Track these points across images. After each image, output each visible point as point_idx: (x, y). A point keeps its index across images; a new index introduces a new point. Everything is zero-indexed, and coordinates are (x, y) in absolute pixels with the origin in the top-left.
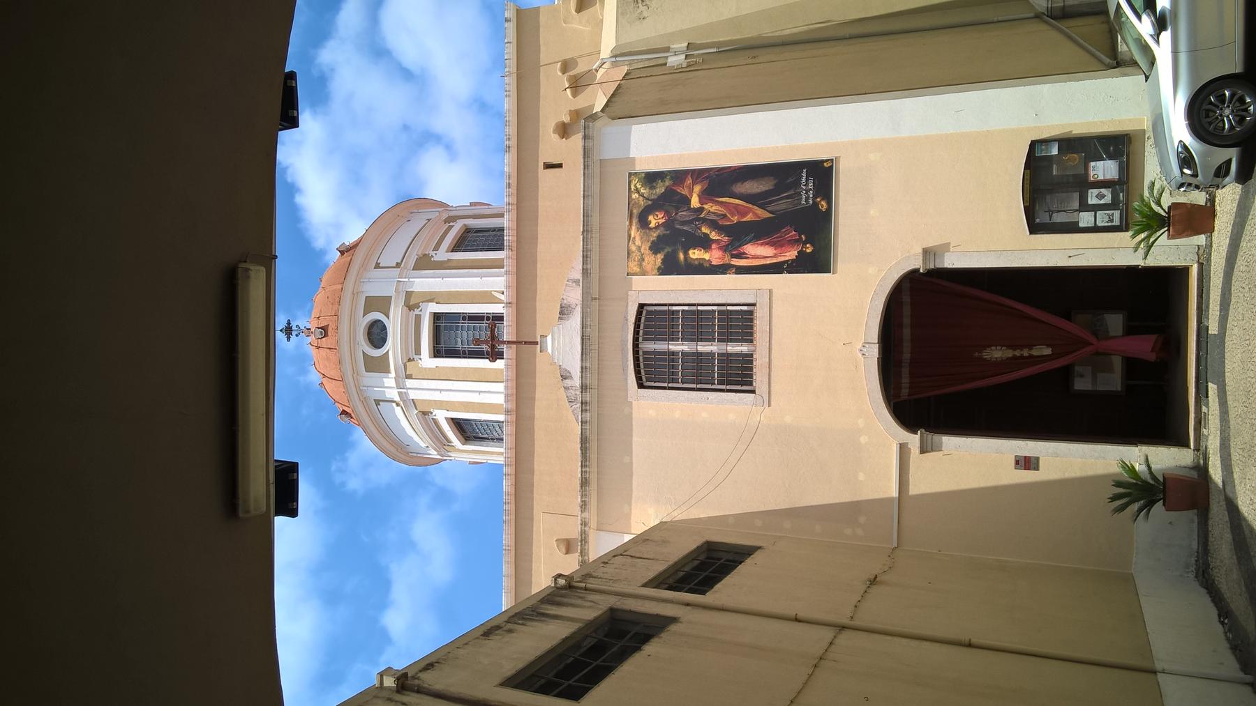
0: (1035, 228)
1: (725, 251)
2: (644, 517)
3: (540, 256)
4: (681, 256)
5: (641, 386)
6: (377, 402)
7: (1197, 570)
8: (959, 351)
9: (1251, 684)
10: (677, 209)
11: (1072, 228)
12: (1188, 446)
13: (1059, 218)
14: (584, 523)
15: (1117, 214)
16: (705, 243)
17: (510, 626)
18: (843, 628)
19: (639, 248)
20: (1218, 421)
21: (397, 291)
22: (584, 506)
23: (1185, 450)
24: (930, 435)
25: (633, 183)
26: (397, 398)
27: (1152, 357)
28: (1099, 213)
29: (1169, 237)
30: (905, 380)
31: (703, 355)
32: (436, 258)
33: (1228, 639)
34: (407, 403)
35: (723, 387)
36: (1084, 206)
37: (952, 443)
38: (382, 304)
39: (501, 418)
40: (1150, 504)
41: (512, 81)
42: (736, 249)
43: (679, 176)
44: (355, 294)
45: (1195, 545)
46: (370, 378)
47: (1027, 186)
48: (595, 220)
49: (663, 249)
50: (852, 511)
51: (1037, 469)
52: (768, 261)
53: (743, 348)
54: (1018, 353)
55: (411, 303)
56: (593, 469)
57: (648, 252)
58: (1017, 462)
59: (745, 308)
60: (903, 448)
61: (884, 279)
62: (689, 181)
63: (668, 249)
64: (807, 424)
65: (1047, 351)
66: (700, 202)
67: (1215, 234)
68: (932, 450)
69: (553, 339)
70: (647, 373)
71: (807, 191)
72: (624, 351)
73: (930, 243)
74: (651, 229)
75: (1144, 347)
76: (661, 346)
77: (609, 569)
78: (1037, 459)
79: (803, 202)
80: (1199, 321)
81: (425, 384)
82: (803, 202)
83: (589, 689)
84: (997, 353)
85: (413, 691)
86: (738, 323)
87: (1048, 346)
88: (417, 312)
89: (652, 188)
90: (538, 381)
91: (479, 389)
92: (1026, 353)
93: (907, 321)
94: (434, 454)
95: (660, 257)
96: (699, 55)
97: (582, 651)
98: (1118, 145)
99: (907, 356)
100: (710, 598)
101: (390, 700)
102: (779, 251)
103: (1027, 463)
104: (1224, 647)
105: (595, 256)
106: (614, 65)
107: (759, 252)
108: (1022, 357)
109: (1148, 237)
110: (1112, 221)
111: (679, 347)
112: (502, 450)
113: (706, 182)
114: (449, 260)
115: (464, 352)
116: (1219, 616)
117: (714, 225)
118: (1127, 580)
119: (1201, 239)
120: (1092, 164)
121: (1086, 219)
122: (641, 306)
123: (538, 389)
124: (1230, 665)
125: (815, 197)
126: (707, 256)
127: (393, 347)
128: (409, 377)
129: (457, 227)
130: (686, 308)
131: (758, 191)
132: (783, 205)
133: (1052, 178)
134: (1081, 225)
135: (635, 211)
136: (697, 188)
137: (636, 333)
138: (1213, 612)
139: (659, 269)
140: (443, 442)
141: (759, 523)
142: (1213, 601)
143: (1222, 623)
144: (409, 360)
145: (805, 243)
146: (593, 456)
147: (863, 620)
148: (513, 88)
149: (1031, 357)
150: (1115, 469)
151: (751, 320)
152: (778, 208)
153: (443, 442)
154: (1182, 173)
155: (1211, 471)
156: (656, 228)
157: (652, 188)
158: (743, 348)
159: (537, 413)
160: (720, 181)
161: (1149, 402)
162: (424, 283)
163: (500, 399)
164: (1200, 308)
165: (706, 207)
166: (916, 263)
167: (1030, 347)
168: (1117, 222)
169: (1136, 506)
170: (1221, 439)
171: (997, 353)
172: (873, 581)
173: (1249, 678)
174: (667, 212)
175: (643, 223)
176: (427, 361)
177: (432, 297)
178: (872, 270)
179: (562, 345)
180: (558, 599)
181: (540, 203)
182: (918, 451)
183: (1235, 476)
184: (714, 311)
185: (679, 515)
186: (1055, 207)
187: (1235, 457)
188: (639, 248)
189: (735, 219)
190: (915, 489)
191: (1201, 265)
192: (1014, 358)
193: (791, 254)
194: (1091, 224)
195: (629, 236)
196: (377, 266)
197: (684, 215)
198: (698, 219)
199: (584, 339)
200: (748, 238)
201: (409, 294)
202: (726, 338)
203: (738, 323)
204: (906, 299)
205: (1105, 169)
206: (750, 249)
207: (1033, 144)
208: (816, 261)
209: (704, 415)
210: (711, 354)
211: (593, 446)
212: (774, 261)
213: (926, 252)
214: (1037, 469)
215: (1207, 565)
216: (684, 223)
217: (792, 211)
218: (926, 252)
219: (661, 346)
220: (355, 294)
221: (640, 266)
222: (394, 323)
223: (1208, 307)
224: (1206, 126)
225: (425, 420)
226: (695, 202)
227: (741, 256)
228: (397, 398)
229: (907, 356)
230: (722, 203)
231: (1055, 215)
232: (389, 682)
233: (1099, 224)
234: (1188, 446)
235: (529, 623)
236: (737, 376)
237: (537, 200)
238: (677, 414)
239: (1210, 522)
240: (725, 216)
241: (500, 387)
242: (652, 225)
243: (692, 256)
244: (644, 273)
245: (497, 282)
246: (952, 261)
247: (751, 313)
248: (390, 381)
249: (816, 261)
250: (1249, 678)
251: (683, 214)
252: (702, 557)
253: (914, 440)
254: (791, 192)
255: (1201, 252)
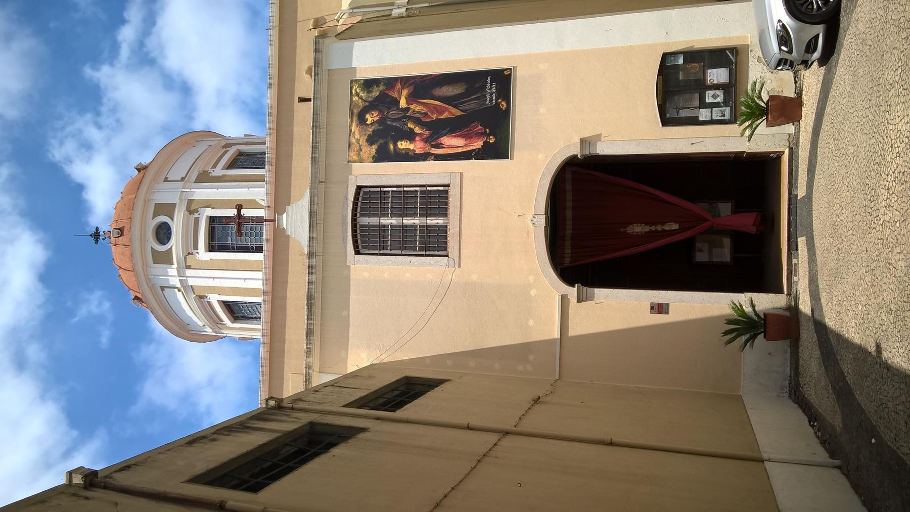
0: (666, 121)
1: (426, 142)
2: (358, 359)
3: (293, 171)
4: (392, 147)
5: (358, 252)
6: (163, 288)
7: (790, 391)
8: (607, 220)
9: (839, 468)
10: (389, 109)
11: (694, 121)
12: (782, 292)
13: (684, 113)
14: (309, 367)
15: (727, 111)
16: (410, 136)
17: (215, 436)
18: (507, 433)
19: (358, 141)
20: (807, 265)
21: (181, 199)
22: (309, 352)
23: (779, 296)
24: (585, 288)
25: (355, 88)
26: (179, 285)
27: (753, 230)
28: (714, 109)
29: (768, 126)
30: (568, 251)
31: (409, 225)
32: (214, 174)
33: (818, 437)
34: (187, 289)
35: (423, 253)
36: (703, 105)
37: (601, 293)
38: (168, 209)
39: (259, 300)
40: (753, 338)
41: (274, 34)
42: (434, 141)
43: (391, 82)
44: (146, 202)
45: (788, 370)
46: (157, 269)
47: (660, 89)
48: (323, 119)
49: (377, 141)
50: (523, 350)
51: (667, 313)
52: (460, 150)
53: (440, 221)
54: (653, 228)
55: (192, 208)
56: (317, 322)
57: (365, 143)
58: (652, 308)
59: (441, 188)
60: (564, 298)
61: (550, 163)
62: (399, 86)
63: (381, 141)
64: (488, 282)
65: (675, 227)
66: (407, 103)
67: (802, 123)
68: (587, 300)
69: (287, 216)
70: (363, 242)
71: (491, 94)
72: (344, 224)
73: (586, 134)
74: (368, 125)
75: (747, 222)
76: (374, 221)
77: (318, 396)
78: (668, 305)
79: (488, 102)
80: (790, 193)
81: (201, 273)
82: (488, 102)
83: (267, 485)
84: (638, 229)
85: (100, 488)
86: (435, 200)
87: (676, 222)
88: (196, 215)
89: (369, 92)
90: (290, 269)
91: (241, 276)
92: (659, 228)
93: (569, 204)
94: (209, 331)
95: (374, 147)
96: (416, 9)
97: (280, 457)
98: (727, 57)
99: (569, 232)
100: (400, 414)
101: (75, 495)
102: (468, 142)
103: (660, 308)
104: (815, 443)
105: (322, 146)
106: (351, 15)
107: (453, 143)
108: (656, 231)
109: (752, 124)
110: (724, 115)
111: (387, 221)
112: (259, 327)
113: (412, 87)
114: (224, 176)
115: (233, 247)
116: (810, 422)
117: (418, 122)
118: (739, 399)
119: (790, 128)
120: (709, 71)
121: (704, 114)
122: (359, 188)
123: (290, 275)
124: (822, 455)
125: (497, 98)
126: (411, 147)
127: (176, 244)
128: (189, 267)
129: (232, 151)
130: (395, 189)
131: (453, 94)
132: (472, 105)
133: (680, 82)
134: (701, 119)
135: (355, 111)
136: (405, 92)
137: (355, 209)
138: (805, 419)
139: (373, 157)
140: (216, 321)
141: (449, 362)
142: (803, 412)
143: (813, 426)
144: (189, 254)
145: (489, 135)
146: (317, 310)
147: (525, 427)
148: (276, 39)
149: (663, 231)
150: (727, 311)
151: (447, 198)
152: (468, 107)
153: (216, 321)
154: (780, 49)
155: (801, 307)
156: (372, 124)
157: (369, 92)
158: (440, 221)
159: (289, 294)
160: (423, 86)
161: (755, 265)
162: (203, 193)
163: (259, 285)
164: (790, 183)
165: (412, 107)
166: (575, 150)
167: (663, 224)
168: (727, 117)
169: (744, 338)
170: (810, 276)
171: (638, 229)
172: (537, 401)
173: (837, 462)
174: (381, 112)
175: (362, 120)
176: (203, 254)
177: (209, 204)
178: (541, 156)
179: (296, 221)
180: (266, 416)
181: (295, 129)
182: (575, 300)
183: (822, 301)
184: (416, 191)
185: (386, 358)
186: (681, 105)
187: (822, 284)
188: (358, 141)
189: (434, 117)
190: (573, 332)
191: (791, 149)
192: (651, 232)
193: (478, 144)
194: (708, 118)
195: (350, 131)
196: (166, 180)
197: (397, 114)
198: (405, 117)
199: (311, 214)
200: (444, 132)
201: (190, 202)
202: (427, 212)
203: (435, 200)
204: (569, 176)
205: (717, 75)
206: (447, 141)
207: (665, 56)
208: (498, 149)
209: (407, 275)
210: (414, 226)
211: (318, 303)
212: (465, 149)
213: (583, 141)
214: (667, 313)
215: (798, 384)
216: (394, 120)
217: (479, 110)
218: (583, 141)
219: (374, 221)
220: (146, 202)
221: (359, 155)
222: (177, 225)
223: (797, 180)
224: (800, 7)
225: (202, 303)
226: (403, 103)
227: (439, 146)
228: (179, 285)
229: (569, 232)
230: (424, 103)
231: (681, 111)
232: (78, 480)
233: (715, 118)
234: (782, 292)
235: (233, 434)
236: (434, 243)
237: (293, 126)
238: (386, 275)
239: (800, 349)
240: (426, 114)
241: (260, 275)
242: (369, 122)
243: (400, 146)
244: (361, 161)
245: (259, 193)
246: (604, 149)
247: (446, 192)
248: (173, 271)
249: (498, 149)
250: (837, 462)
251: (393, 113)
252: (403, 388)
253: (572, 292)
254: (479, 95)
255: (791, 139)
